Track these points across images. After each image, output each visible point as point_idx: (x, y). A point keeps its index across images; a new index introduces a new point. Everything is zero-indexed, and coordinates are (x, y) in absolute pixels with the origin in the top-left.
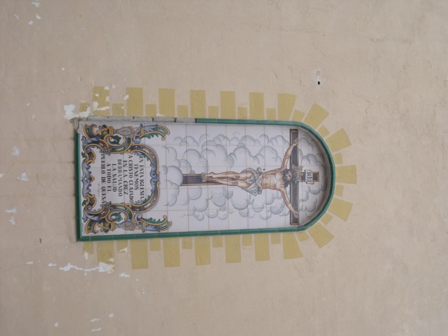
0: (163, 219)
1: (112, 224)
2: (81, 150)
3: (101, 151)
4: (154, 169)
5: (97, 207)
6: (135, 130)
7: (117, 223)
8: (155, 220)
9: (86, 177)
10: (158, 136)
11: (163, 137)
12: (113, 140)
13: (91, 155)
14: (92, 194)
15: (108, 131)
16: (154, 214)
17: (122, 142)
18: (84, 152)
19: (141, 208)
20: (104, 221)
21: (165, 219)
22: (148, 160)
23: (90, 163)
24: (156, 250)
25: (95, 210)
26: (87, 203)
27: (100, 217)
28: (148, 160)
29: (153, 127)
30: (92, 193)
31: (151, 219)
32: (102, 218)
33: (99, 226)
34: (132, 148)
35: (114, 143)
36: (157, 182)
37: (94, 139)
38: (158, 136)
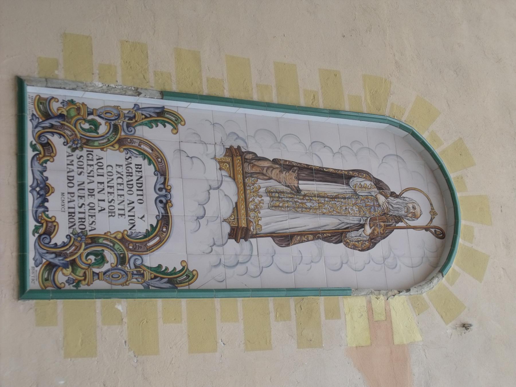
0: (181, 267)
1: (87, 273)
2: (30, 138)
3: (65, 144)
4: (162, 180)
5: (59, 238)
6: (126, 112)
7: (96, 270)
8: (167, 268)
9: (38, 185)
10: (165, 126)
11: (175, 129)
12: (87, 126)
13: (47, 146)
14: (50, 216)
15: (79, 109)
16: (166, 256)
17: (103, 129)
18: (34, 142)
19: (143, 243)
20: (73, 263)
21: (184, 267)
22: (150, 164)
23: (46, 162)
24: (171, 316)
25: (56, 244)
26: (41, 231)
27: (66, 258)
28: (150, 164)
29: (158, 111)
30: (50, 214)
31: (160, 266)
32: (68, 260)
33: (63, 274)
34: (121, 142)
35: (89, 131)
36: (167, 202)
37: (53, 122)
38: (165, 126)
